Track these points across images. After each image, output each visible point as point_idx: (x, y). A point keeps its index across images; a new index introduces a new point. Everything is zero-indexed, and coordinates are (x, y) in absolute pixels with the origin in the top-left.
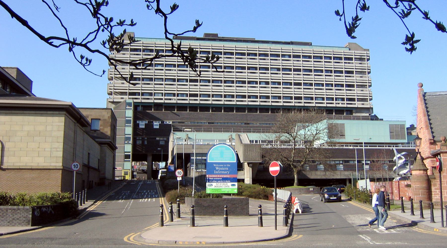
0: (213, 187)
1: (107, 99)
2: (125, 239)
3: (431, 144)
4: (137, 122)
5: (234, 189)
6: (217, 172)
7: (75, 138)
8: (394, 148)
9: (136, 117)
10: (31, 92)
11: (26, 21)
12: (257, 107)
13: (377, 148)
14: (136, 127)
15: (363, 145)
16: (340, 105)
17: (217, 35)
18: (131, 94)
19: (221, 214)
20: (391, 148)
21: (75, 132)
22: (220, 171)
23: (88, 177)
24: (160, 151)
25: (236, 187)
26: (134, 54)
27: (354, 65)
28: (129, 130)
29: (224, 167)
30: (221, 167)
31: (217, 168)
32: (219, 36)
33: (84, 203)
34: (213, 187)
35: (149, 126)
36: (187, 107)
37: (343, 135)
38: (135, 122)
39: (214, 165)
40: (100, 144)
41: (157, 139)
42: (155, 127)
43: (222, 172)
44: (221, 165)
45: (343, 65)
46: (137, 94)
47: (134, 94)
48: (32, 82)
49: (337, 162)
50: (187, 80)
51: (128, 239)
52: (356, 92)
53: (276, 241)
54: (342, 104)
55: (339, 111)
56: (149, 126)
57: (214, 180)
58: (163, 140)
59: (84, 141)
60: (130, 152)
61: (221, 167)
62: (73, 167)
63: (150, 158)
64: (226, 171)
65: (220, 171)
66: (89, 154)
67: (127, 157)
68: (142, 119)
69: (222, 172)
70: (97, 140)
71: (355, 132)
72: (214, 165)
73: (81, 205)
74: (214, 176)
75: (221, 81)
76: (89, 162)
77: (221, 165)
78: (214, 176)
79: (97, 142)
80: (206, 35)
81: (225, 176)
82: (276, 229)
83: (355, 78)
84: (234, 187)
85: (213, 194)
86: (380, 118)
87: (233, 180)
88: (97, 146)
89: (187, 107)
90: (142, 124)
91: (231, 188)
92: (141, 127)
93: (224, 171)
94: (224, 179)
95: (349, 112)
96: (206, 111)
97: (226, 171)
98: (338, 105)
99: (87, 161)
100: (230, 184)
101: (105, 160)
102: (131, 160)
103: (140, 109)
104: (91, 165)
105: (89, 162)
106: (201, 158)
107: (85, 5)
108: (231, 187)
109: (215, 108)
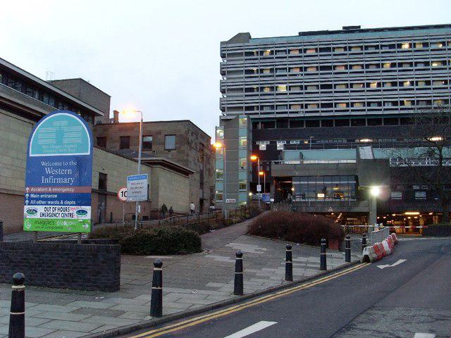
0: (38, 214)
1: (220, 117)
5: (84, 222)
6: (47, 181)
9: (256, 136)
22: (56, 176)
25: (88, 216)
26: (250, 59)
29: (62, 167)
30: (58, 167)
31: (48, 171)
34: (37, 216)
36: (364, 120)
39: (43, 164)
43: (59, 180)
44: (56, 164)
47: (252, 108)
48: (110, 97)
56: (272, 147)
57: (37, 199)
61: (58, 167)
64: (67, 176)
65: (56, 176)
68: (263, 139)
69: (59, 180)
72: (43, 164)
74: (39, 190)
77: (56, 164)
78: (39, 190)
80: (344, 28)
81: (64, 190)
83: (241, 80)
84: (82, 218)
92: (261, 149)
93: (63, 176)
94: (63, 198)
96: (345, 125)
97: (67, 176)
100: (74, 209)
103: (260, 126)
106: (346, 182)
108: (75, 216)
109: (357, 120)
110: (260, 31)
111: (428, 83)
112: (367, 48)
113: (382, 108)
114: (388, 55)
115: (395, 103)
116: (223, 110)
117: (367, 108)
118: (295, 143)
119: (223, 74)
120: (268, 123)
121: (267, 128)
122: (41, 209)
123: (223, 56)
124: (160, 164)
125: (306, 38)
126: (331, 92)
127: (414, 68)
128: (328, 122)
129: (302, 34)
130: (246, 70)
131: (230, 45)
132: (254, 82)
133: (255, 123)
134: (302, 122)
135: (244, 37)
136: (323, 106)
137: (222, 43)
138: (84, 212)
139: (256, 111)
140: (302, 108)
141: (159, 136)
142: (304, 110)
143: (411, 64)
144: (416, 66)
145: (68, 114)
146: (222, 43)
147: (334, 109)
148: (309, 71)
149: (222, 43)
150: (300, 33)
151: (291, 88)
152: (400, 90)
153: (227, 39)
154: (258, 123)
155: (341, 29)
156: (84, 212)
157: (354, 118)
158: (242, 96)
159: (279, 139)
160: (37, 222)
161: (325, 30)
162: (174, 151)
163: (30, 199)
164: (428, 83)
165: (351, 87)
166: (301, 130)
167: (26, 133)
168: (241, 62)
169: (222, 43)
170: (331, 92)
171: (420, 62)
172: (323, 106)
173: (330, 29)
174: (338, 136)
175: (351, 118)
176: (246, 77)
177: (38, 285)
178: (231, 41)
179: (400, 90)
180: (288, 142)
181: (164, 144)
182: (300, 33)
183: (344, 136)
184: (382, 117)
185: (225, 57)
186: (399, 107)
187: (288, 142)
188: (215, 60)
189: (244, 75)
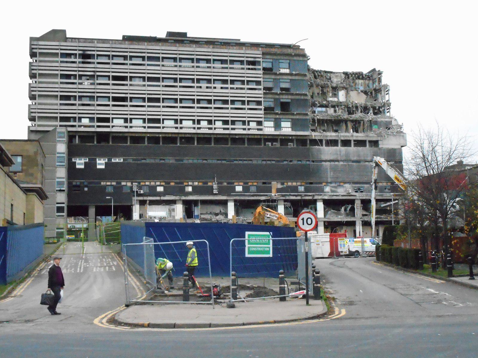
1: (29, 127)
3: (283, 299)
4: (73, 160)
9: (72, 152)
11: (53, 30)
12: (243, 137)
14: (71, 167)
17: (184, 35)
18: (63, 119)
24: (110, 201)
26: (67, 62)
28: (62, 173)
32: (188, 36)
35: (91, 165)
38: (70, 160)
40: (27, 191)
41: (102, 183)
42: (99, 167)
46: (72, 119)
47: (67, 119)
50: (144, 99)
56: (91, 165)
58: (111, 185)
60: (64, 203)
63: (92, 211)
66: (12, 205)
68: (80, 155)
70: (22, 185)
75: (75, 97)
79: (21, 188)
80: (170, 34)
82: (12, 205)
83: (58, 86)
95: (373, 144)
99: (10, 216)
102: (65, 214)
116: (32, 119)
118: (117, 161)
120: (86, 137)
125: (127, 45)
126: (159, 107)
127: (178, 84)
130: (61, 75)
131: (41, 43)
133: (71, 136)
134: (193, 139)
135: (57, 35)
139: (72, 123)
140: (194, 123)
144: (131, 80)
145: (171, 145)
146: (32, 39)
149: (32, 39)
150: (124, 37)
151: (165, 100)
152: (232, 108)
153: (38, 35)
154: (75, 137)
155: (163, 35)
157: (183, 136)
158: (57, 104)
161: (153, 35)
162: (21, 174)
165: (181, 102)
166: (124, 147)
167: (444, 214)
168: (57, 65)
170: (159, 107)
175: (247, 137)
176: (61, 83)
178: (44, 38)
179: (232, 108)
180: (110, 160)
182: (124, 37)
183: (172, 155)
184: (262, 137)
187: (110, 160)
189: (59, 80)
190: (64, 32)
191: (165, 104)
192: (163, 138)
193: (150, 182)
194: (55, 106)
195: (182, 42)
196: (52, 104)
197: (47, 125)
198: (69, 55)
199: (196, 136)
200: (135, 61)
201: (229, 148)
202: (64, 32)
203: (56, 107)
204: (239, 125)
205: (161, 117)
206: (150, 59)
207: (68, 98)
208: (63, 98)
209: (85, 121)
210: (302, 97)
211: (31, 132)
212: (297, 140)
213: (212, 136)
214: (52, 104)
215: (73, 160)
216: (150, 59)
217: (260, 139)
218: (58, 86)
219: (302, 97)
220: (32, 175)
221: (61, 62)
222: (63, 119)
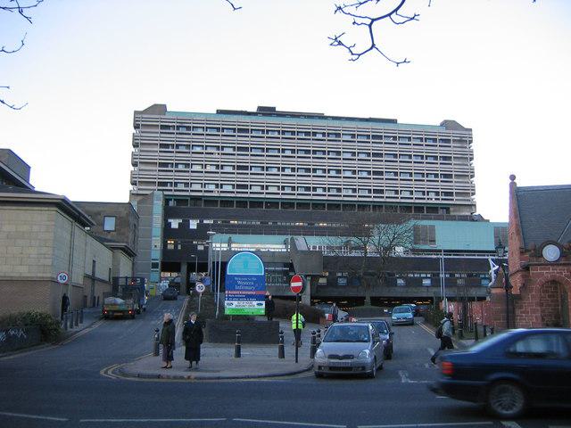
0: (234, 306)
2: (102, 372)
3: (522, 253)
5: (261, 309)
7: (72, 242)
8: (490, 258)
9: (168, 213)
10: (28, 183)
13: (477, 257)
15: (443, 253)
16: (434, 201)
18: (160, 184)
19: (231, 341)
20: (486, 257)
21: (72, 235)
23: (93, 291)
24: (194, 258)
27: (452, 150)
33: (77, 325)
34: (234, 306)
35: (184, 225)
36: (278, 203)
37: (433, 241)
39: (236, 278)
40: (112, 249)
42: (191, 228)
45: (439, 151)
47: (165, 184)
48: (30, 167)
49: (422, 275)
51: (106, 372)
52: (455, 185)
53: (286, 377)
54: (436, 199)
55: (433, 209)
56: (184, 225)
59: (86, 245)
62: (59, 278)
63: (184, 268)
66: (297, 362)
67: (155, 266)
71: (448, 236)
72: (236, 278)
73: (71, 327)
74: (235, 292)
76: (93, 273)
78: (235, 292)
79: (106, 246)
80: (260, 108)
82: (297, 362)
83: (156, 154)
85: (233, 316)
86: (485, 218)
87: (258, 298)
88: (108, 253)
89: (278, 203)
90: (175, 224)
91: (256, 308)
94: (249, 297)
98: (430, 201)
100: (255, 303)
101: (119, 269)
103: (171, 203)
104: (98, 275)
105: (93, 273)
107: (359, 55)
108: (256, 306)
110: (180, 103)
111: (339, 171)
112: (284, 132)
113: (296, 192)
114: (303, 141)
115: (308, 189)
116: (134, 183)
117: (281, 192)
119: (135, 146)
120: (181, 201)
121: (177, 206)
122: (235, 303)
123: (136, 127)
124: (121, 249)
125: (224, 117)
128: (242, 203)
129: (220, 112)
132: (171, 156)
133: (167, 201)
135: (159, 109)
136: (239, 186)
137: (136, 113)
138: (261, 304)
139: (169, 188)
141: (99, 217)
142: (220, 190)
143: (324, 152)
146: (136, 112)
147: (249, 190)
148: (226, 151)
149: (136, 112)
153: (141, 109)
155: (255, 110)
156: (261, 304)
159: (193, 218)
160: (233, 309)
163: (229, 297)
164: (339, 171)
168: (157, 136)
169: (136, 113)
171: (302, 132)
172: (239, 186)
173: (453, 249)
174: (252, 218)
177: (18, 349)
178: (146, 111)
181: (103, 225)
183: (258, 218)
185: (139, 128)
186: (312, 193)
188: (126, 131)
189: (158, 149)
190: (165, 106)
191: (299, 173)
192: (237, 202)
193: (230, 242)
194: (155, 173)
195: (270, 115)
196: (152, 171)
197: (147, 190)
198: (168, 127)
199: (280, 201)
200: (225, 133)
201: (311, 213)
202: (165, 106)
203: (155, 173)
204: (302, 191)
205: (249, 184)
206: (240, 130)
207: (166, 165)
208: (161, 165)
209: (320, 191)
210: (240, 171)
211: (132, 195)
212: (386, 207)
213: (357, 204)
214: (152, 171)
215: (170, 221)
216: (240, 130)
217: (339, 205)
218: (156, 154)
219: (240, 171)
220: (123, 234)
221: (161, 133)
222: (160, 184)
